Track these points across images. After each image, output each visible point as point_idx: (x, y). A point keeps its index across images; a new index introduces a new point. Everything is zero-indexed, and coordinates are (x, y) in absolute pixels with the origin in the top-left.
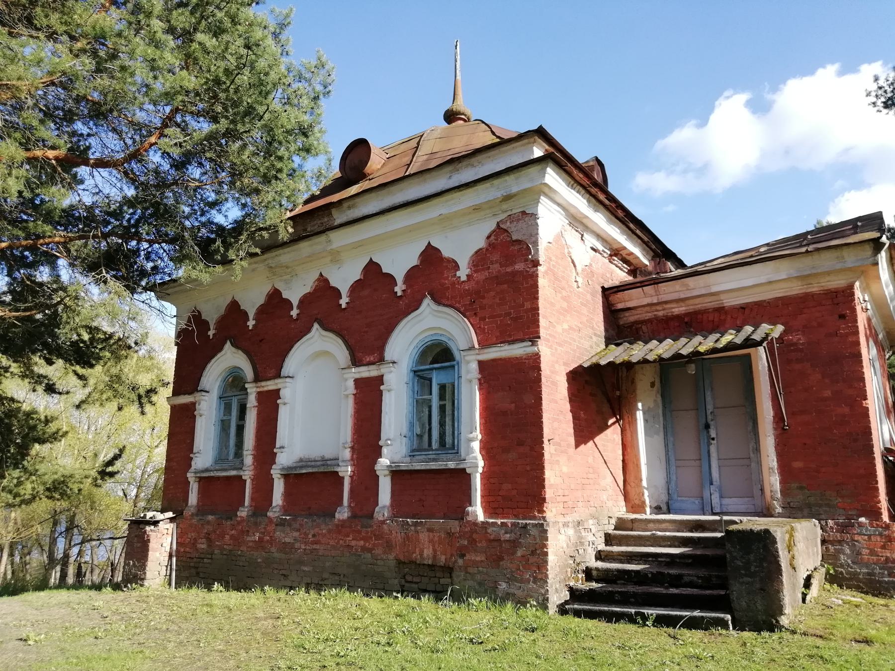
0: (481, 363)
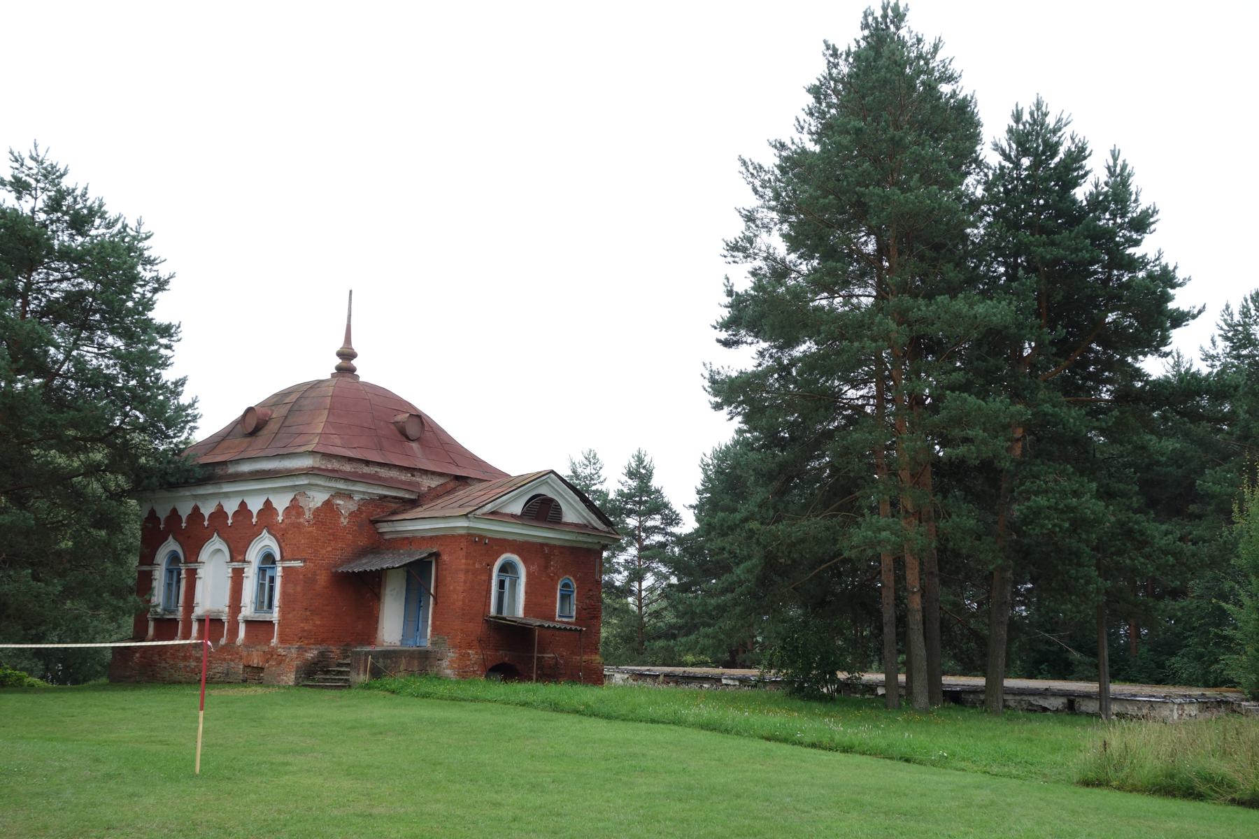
0: (284, 568)
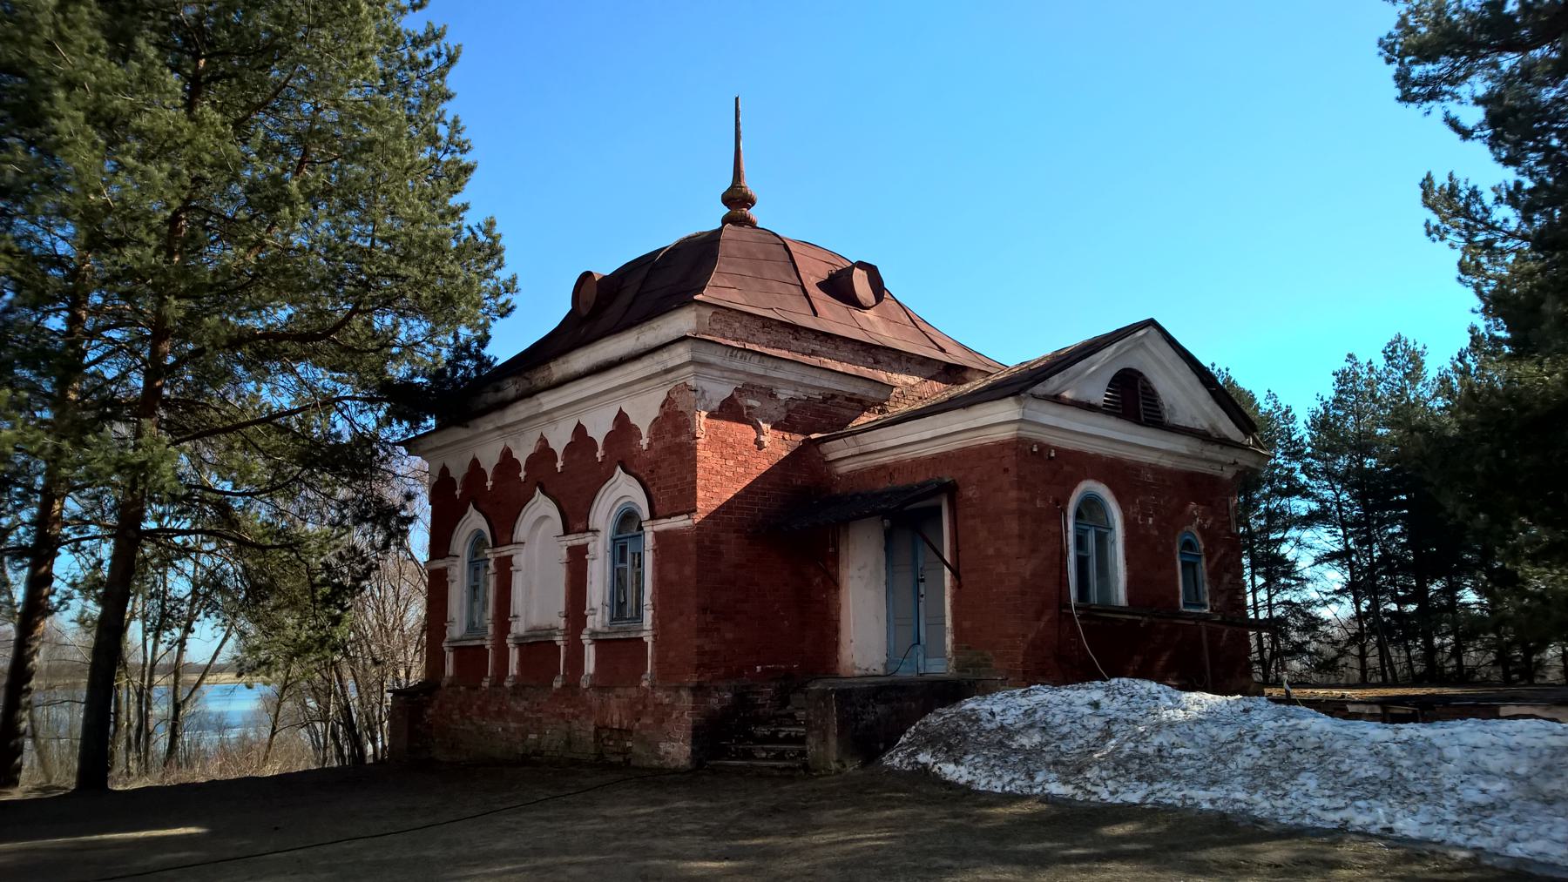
0: (657, 535)
